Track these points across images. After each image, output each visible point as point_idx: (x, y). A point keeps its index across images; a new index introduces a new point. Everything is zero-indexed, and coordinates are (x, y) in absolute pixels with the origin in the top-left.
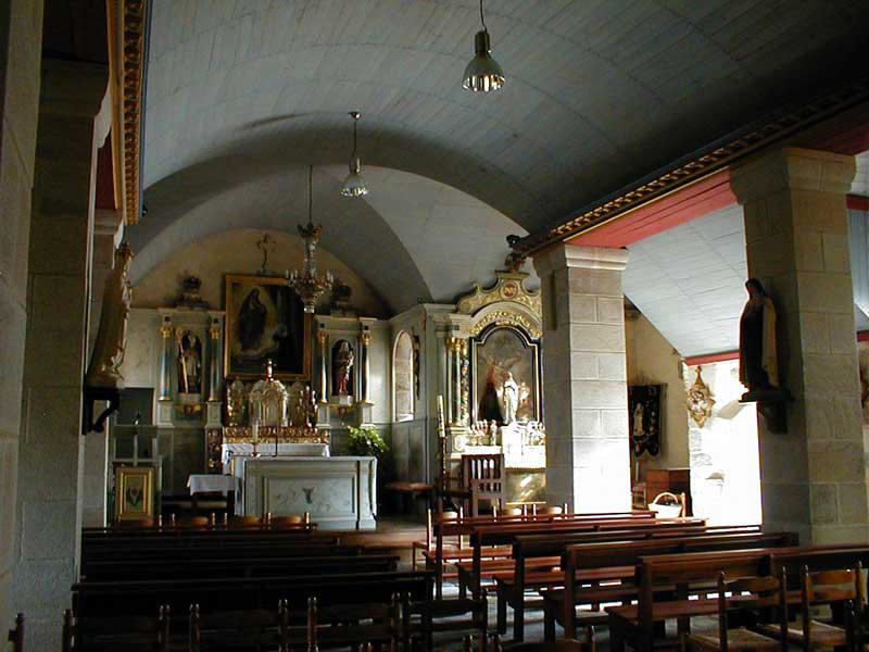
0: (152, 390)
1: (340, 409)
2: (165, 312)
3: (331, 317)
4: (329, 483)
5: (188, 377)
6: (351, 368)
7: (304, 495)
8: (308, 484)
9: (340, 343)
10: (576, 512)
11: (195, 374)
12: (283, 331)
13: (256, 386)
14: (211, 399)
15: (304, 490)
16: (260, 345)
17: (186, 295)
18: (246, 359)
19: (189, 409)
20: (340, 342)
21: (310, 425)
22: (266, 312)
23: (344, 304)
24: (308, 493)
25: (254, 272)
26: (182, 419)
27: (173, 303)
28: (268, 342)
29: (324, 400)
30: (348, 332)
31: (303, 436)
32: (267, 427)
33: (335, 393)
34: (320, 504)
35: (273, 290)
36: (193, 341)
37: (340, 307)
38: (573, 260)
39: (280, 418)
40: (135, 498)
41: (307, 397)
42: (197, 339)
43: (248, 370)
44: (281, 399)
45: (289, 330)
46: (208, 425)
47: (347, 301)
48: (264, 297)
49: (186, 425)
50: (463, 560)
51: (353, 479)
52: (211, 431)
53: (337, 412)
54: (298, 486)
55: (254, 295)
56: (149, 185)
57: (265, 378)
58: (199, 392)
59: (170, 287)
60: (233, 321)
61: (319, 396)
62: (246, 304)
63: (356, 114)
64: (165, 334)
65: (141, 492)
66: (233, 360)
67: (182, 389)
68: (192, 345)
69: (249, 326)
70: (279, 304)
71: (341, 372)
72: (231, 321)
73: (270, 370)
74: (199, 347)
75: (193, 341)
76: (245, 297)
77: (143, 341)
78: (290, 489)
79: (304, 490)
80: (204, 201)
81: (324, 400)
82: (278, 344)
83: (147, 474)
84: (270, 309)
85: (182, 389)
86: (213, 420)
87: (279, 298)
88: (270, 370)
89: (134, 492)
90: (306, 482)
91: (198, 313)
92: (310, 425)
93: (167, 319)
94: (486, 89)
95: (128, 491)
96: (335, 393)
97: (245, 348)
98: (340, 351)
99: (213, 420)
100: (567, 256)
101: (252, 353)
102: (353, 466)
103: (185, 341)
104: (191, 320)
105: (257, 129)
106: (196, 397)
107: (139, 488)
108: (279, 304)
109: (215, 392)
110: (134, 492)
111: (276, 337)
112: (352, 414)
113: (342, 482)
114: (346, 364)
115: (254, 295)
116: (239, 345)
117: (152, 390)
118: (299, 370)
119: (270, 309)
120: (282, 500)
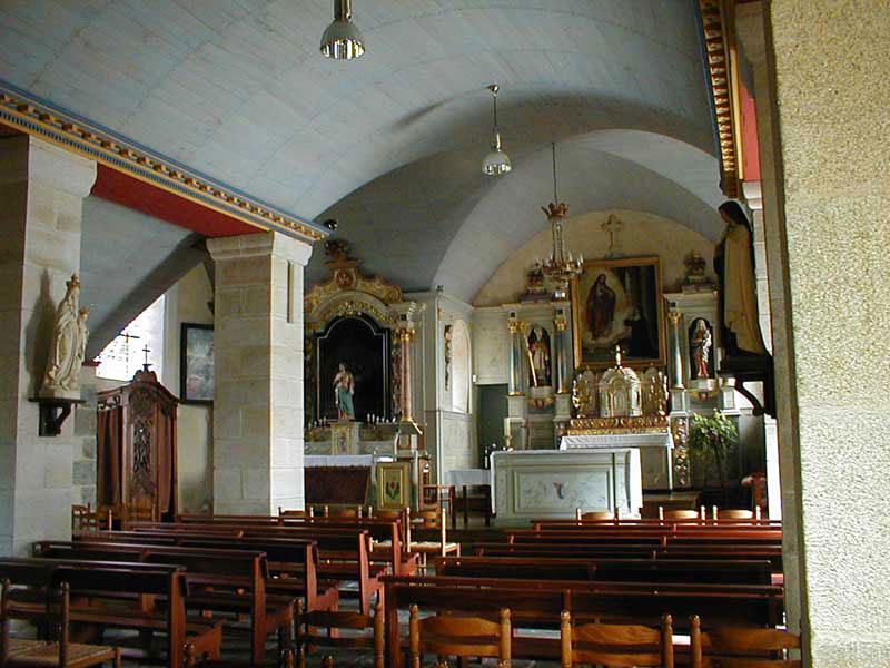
0: (507, 385)
1: (700, 394)
2: (516, 308)
3: (682, 295)
4: (582, 477)
5: (536, 370)
6: (711, 348)
7: (555, 489)
8: (558, 478)
9: (695, 323)
10: (771, 519)
11: (543, 367)
12: (634, 315)
13: (606, 375)
14: (560, 391)
15: (556, 485)
16: (610, 332)
17: (531, 289)
18: (598, 348)
19: (540, 403)
20: (695, 323)
21: (663, 413)
22: (614, 298)
23: (697, 278)
24: (559, 488)
25: (602, 256)
26: (534, 413)
27: (522, 297)
28: (618, 327)
29: (680, 385)
30: (705, 309)
31: (653, 425)
32: (614, 418)
33: (694, 377)
34: (573, 500)
35: (620, 273)
36: (539, 334)
37: (694, 282)
38: (215, 254)
39: (629, 407)
40: (393, 491)
41: (659, 383)
42: (544, 331)
43: (597, 359)
44: (629, 387)
45: (641, 314)
46: (558, 418)
47: (540, 285)
48: (611, 281)
49: (537, 418)
50: (348, 562)
51: (608, 473)
52: (559, 423)
53: (696, 395)
54: (549, 479)
55: (600, 280)
56: (174, 228)
57: (613, 364)
58: (550, 385)
59: (518, 282)
60: (581, 309)
61: (675, 381)
62: (594, 289)
63: (493, 87)
64: (512, 329)
65: (398, 487)
66: (584, 350)
67: (532, 384)
68: (539, 339)
69: (598, 311)
70: (628, 284)
71: (697, 353)
72: (579, 310)
73: (618, 357)
74: (541, 339)
75: (539, 334)
76: (592, 283)
77: (496, 339)
78: (540, 483)
79: (556, 485)
80: (478, 200)
81: (680, 385)
82: (630, 329)
83: (403, 468)
84: (620, 295)
85: (532, 384)
86: (562, 414)
87: (628, 279)
88: (618, 357)
89: (393, 485)
90: (556, 476)
91: (542, 306)
92: (663, 413)
93: (513, 315)
94: (350, 55)
95: (388, 484)
96: (694, 377)
97: (595, 337)
98: (697, 330)
99: (562, 414)
100: (747, 197)
101: (602, 340)
102: (609, 459)
103: (532, 338)
104: (538, 314)
105: (420, 125)
106: (546, 390)
107: (396, 482)
108: (628, 284)
109: (563, 384)
110: (393, 485)
111: (627, 322)
112: (715, 398)
113: (600, 476)
114: (702, 345)
115: (600, 280)
116: (590, 334)
117: (507, 385)
118: (654, 354)
119: (620, 295)
120: (533, 494)
